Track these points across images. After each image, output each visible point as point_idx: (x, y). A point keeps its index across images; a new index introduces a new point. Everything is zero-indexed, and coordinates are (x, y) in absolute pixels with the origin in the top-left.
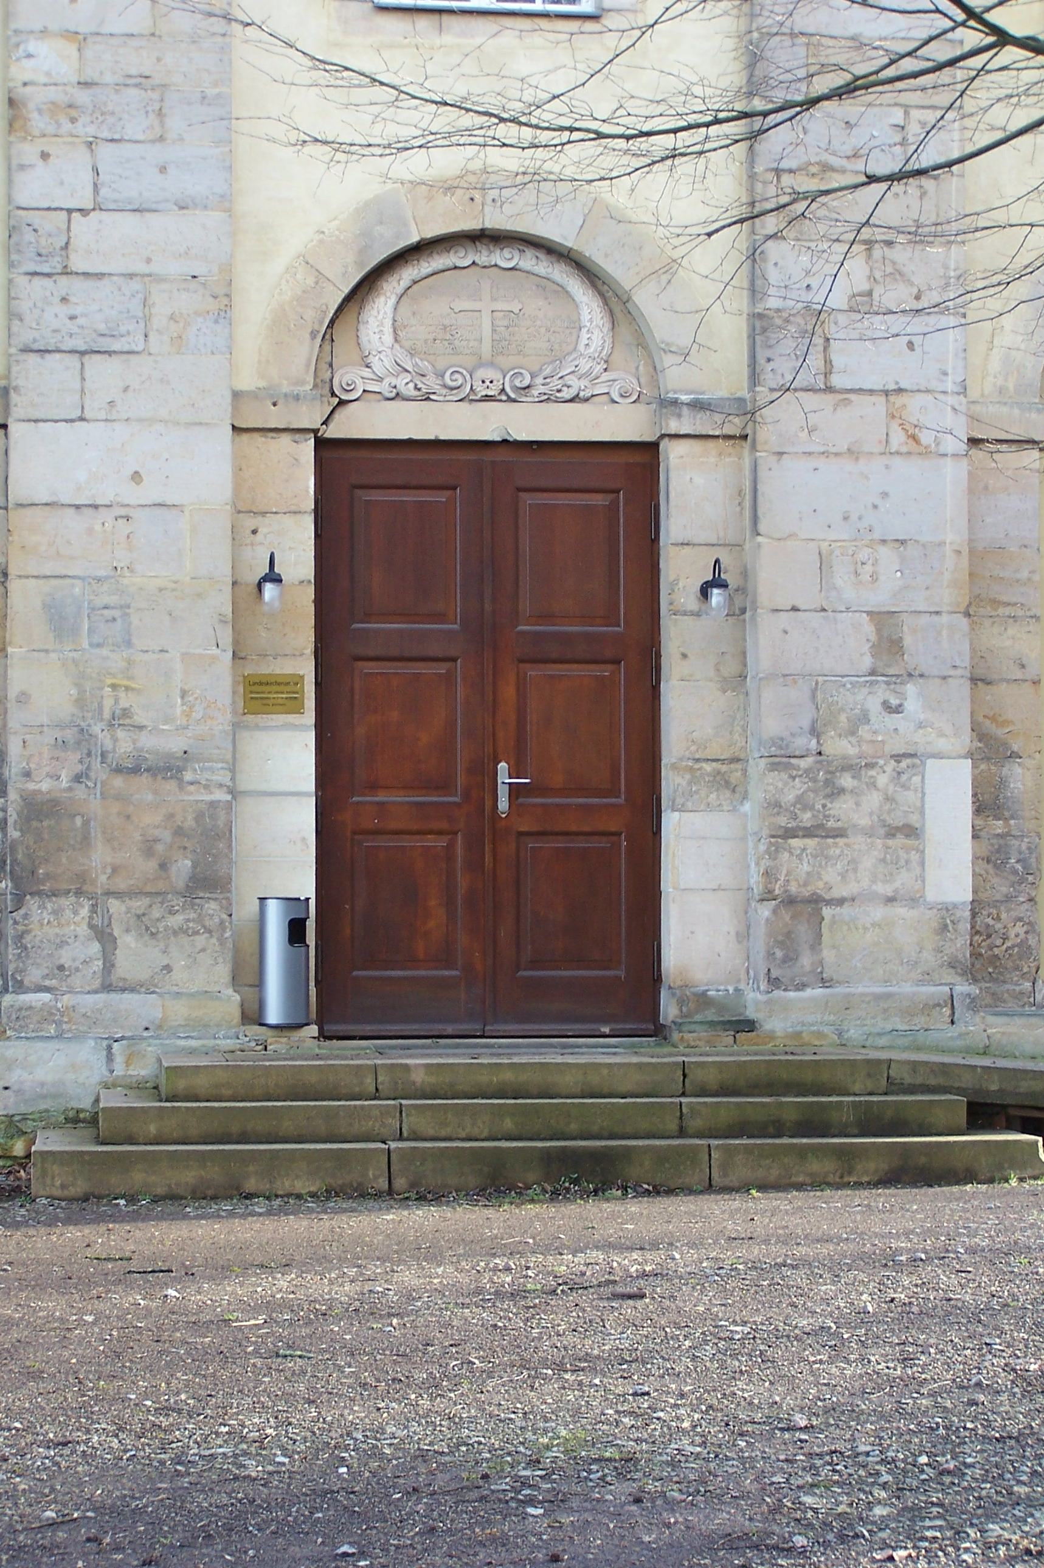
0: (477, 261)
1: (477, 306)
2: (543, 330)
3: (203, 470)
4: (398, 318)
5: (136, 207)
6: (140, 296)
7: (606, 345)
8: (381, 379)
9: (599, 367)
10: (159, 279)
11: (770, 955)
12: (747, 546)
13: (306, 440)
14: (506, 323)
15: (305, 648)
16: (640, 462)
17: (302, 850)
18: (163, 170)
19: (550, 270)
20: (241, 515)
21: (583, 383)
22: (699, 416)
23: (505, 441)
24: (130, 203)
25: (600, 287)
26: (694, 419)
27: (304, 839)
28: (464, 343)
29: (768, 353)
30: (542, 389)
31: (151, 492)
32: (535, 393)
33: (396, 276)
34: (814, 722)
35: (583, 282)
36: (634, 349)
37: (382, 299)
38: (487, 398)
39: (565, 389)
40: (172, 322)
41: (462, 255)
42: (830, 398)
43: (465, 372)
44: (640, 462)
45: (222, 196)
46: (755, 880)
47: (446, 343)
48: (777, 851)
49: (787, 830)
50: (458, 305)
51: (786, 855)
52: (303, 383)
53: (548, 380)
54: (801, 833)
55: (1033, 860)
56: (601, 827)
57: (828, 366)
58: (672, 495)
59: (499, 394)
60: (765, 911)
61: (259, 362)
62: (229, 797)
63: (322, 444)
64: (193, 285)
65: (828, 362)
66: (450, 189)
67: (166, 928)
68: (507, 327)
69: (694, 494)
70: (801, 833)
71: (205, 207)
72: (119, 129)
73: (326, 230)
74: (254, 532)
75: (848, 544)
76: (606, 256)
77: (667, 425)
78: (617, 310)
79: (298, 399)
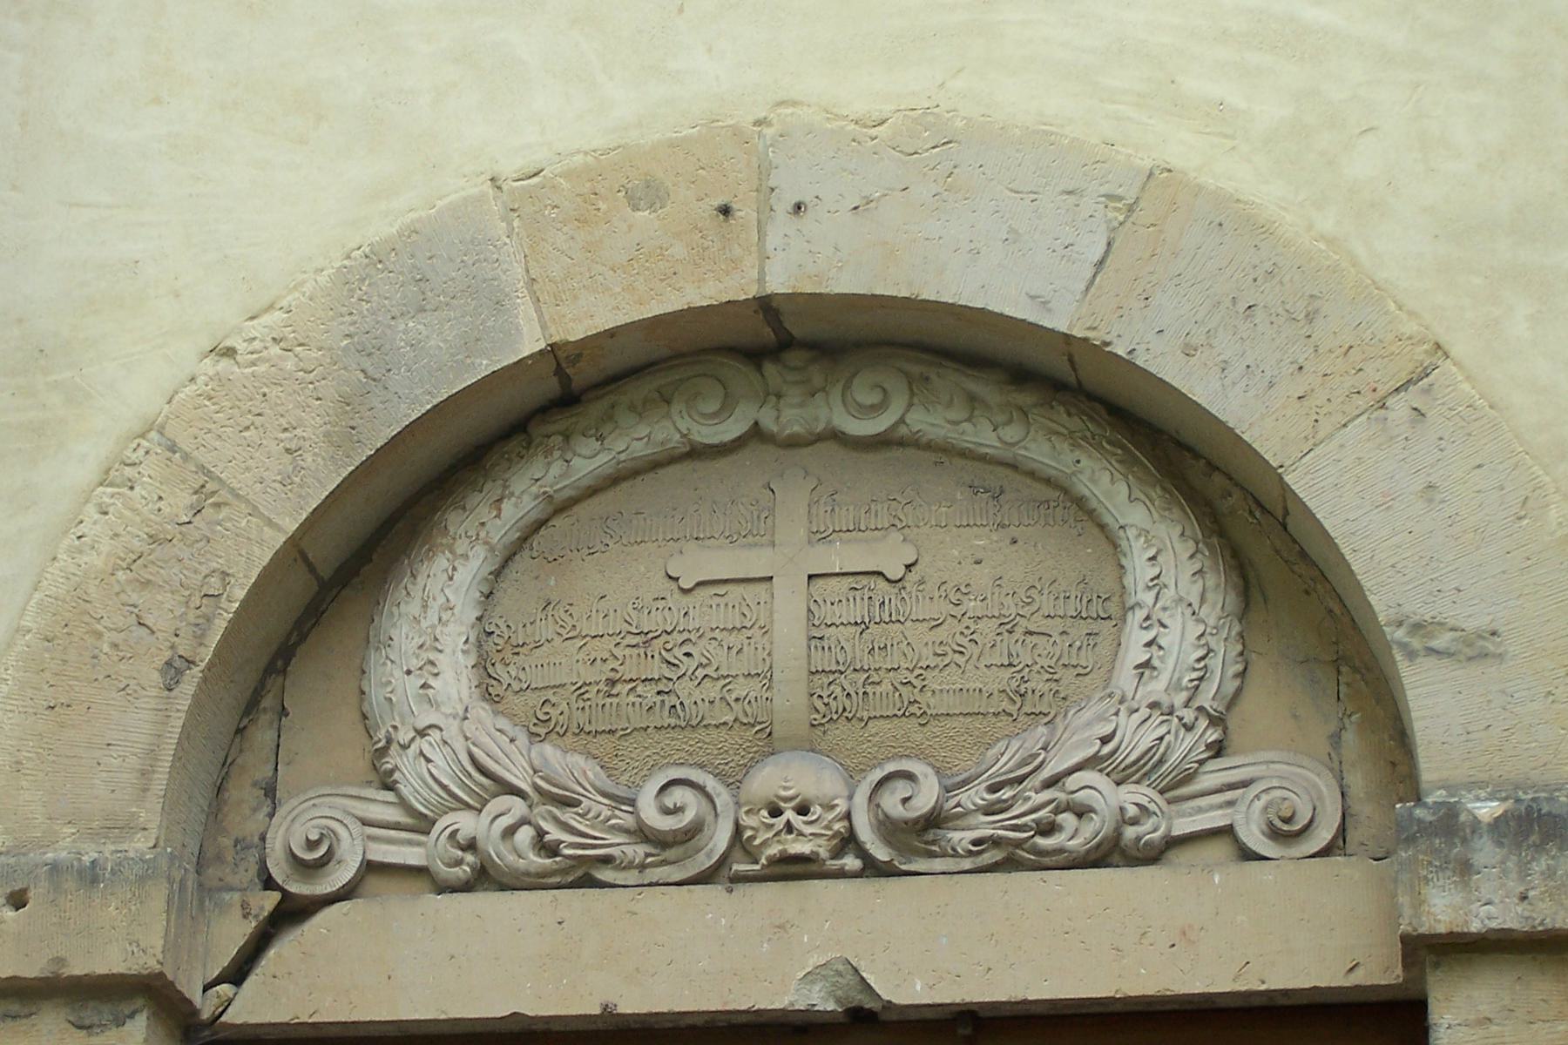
0: (768, 422)
1: (755, 562)
2: (988, 628)
4: (497, 622)
7: (1216, 663)
8: (422, 824)
9: (1189, 739)
13: (119, 1022)
14: (857, 611)
19: (1012, 433)
21: (1132, 796)
22: (1541, 865)
26: (1524, 872)
28: (712, 690)
30: (985, 827)
32: (961, 838)
33: (492, 489)
35: (1128, 462)
37: (442, 562)
38: (793, 868)
39: (1067, 819)
41: (712, 406)
43: (711, 783)
47: (649, 691)
50: (696, 564)
52: (128, 828)
53: (1006, 794)
59: (837, 853)
66: (647, 195)
68: (862, 625)
73: (241, 346)
77: (1419, 903)
79: (95, 881)
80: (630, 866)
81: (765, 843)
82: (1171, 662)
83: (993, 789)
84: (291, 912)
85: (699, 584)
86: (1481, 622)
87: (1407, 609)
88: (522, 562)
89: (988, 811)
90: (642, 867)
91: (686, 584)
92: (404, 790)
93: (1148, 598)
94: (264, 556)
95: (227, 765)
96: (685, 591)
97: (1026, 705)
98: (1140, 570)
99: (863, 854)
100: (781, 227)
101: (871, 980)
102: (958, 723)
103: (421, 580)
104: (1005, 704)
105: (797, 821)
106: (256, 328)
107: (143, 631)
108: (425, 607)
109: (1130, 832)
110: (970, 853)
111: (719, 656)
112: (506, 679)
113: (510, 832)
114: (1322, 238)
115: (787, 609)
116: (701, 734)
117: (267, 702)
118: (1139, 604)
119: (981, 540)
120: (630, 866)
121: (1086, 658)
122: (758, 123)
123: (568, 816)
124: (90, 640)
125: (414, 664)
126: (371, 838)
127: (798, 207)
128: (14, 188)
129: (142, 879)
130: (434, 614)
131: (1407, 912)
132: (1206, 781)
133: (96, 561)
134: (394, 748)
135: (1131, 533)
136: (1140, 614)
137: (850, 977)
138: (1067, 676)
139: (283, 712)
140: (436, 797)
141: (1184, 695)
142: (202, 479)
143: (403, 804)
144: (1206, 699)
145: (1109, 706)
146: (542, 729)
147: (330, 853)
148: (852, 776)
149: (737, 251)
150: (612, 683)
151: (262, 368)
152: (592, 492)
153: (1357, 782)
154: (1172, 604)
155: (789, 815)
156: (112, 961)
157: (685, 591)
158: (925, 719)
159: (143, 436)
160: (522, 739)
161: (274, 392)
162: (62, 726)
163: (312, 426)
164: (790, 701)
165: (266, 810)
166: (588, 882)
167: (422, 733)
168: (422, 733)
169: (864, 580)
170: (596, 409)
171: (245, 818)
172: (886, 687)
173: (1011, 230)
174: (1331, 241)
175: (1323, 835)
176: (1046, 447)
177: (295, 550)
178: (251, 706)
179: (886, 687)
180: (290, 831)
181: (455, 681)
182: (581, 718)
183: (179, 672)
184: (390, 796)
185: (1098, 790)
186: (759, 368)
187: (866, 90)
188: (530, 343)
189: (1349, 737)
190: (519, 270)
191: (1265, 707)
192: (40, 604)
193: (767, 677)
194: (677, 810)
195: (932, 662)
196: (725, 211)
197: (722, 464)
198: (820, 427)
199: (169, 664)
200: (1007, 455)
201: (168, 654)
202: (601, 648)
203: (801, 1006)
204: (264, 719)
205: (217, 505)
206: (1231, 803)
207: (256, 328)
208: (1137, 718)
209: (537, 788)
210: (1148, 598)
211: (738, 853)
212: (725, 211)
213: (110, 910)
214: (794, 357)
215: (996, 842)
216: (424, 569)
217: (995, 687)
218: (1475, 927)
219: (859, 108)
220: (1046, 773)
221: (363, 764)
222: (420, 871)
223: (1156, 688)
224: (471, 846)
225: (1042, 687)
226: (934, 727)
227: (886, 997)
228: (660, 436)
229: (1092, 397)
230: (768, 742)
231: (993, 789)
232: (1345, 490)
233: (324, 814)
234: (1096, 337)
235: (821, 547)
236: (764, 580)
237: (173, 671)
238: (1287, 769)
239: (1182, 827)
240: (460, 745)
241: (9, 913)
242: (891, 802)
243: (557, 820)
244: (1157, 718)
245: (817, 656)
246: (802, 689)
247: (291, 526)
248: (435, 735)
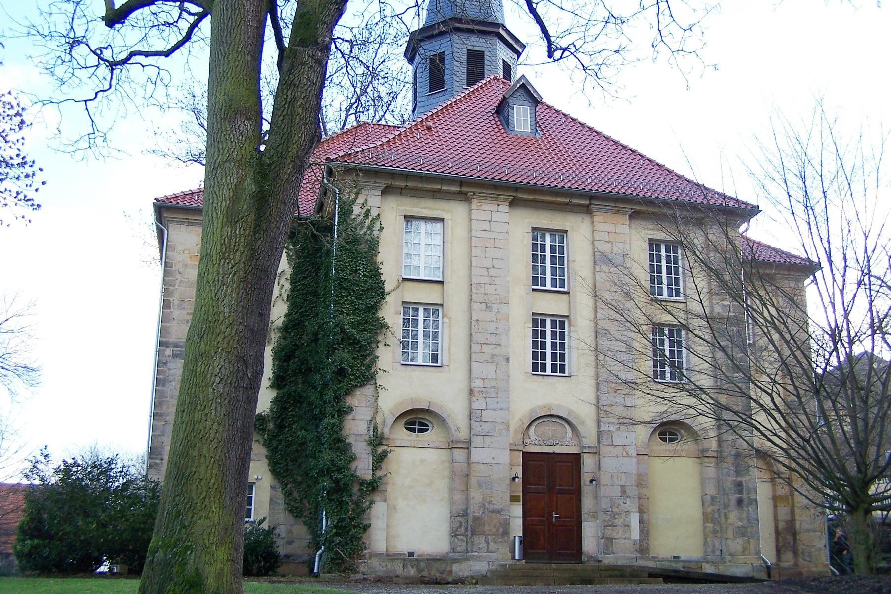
44: (576, 458)
46: (600, 534)
69: (588, 464)
232: (579, 428)
236: (549, 428)
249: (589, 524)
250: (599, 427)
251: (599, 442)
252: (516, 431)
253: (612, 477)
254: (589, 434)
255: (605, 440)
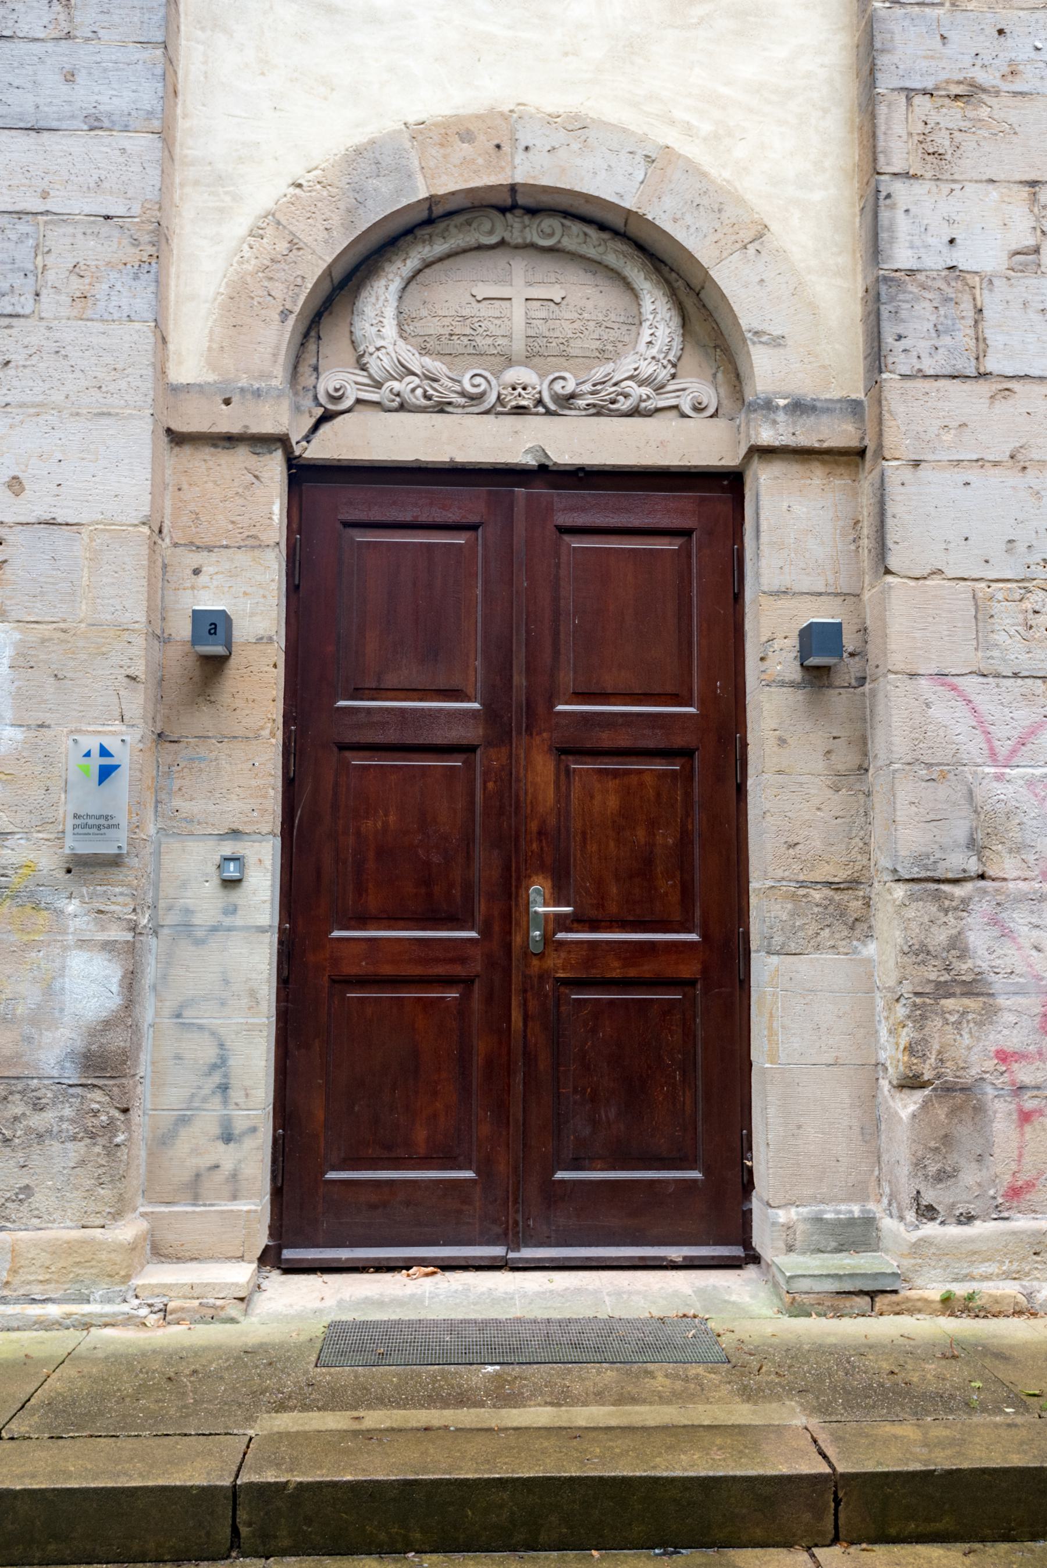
0: (508, 238)
2: (592, 324)
3: (114, 475)
4: (405, 308)
5: (29, 126)
6: (31, 242)
8: (378, 385)
9: (665, 372)
10: (60, 218)
11: (919, 1164)
12: (866, 596)
13: (271, 453)
14: (543, 314)
15: (262, 728)
16: (719, 493)
17: (250, 1008)
18: (70, 77)
20: (178, 550)
21: (645, 391)
22: (801, 421)
23: (543, 468)
24: (21, 120)
25: (667, 275)
27: (252, 993)
28: (489, 341)
29: (900, 330)
31: (35, 505)
32: (581, 403)
34: (973, 831)
36: (711, 351)
37: (383, 282)
38: (520, 410)
39: (621, 398)
40: (74, 278)
42: (984, 388)
44: (719, 493)
45: (149, 113)
46: (891, 1052)
47: (465, 340)
48: (923, 1017)
49: (938, 984)
50: (483, 290)
51: (938, 1022)
52: (270, 376)
53: (599, 387)
54: (958, 991)
55: (193, 863)
56: (670, 972)
57: (982, 346)
58: (764, 526)
60: (906, 1106)
61: (210, 349)
62: (129, 936)
63: (303, 476)
64: (106, 228)
65: (980, 339)
66: (467, 137)
67: (29, 1130)
69: (792, 545)
70: (958, 991)
71: (126, 129)
72: (10, 23)
73: (305, 184)
74: (197, 572)
75: (1014, 585)
76: (675, 220)
77: (757, 434)
78: (689, 303)
79: (259, 396)
80: (459, 406)
81: (510, 400)
82: (659, 342)
83: (594, 385)
84: (327, 417)
85: (485, 299)
86: (779, 333)
87: (753, 326)
88: (413, 286)
89: (592, 393)
90: (464, 407)
91: (479, 299)
92: (372, 371)
93: (651, 317)
94: (319, 272)
95: (298, 357)
96: (479, 301)
97: (603, 355)
98: (647, 306)
99: (545, 407)
100: (520, 157)
101: (549, 454)
102: (580, 360)
103: (375, 288)
104: (597, 354)
105: (523, 392)
106: (311, 176)
107: (270, 298)
108: (377, 299)
109: (643, 405)
110: (585, 409)
111: (492, 328)
112: (409, 331)
113: (413, 390)
114: (725, 180)
115: (518, 311)
116: (484, 357)
117: (313, 333)
118: (648, 319)
119: (589, 291)
120: (459, 406)
121: (626, 339)
122: (511, 111)
123: (435, 385)
124: (249, 300)
125: (374, 322)
126: (358, 389)
127: (527, 148)
128: (204, 105)
129: (279, 396)
130: (380, 305)
131: (753, 436)
132: (669, 388)
133: (249, 268)
134: (367, 355)
135: (645, 292)
136: (648, 323)
137: (541, 453)
138: (620, 345)
139: (319, 338)
140: (384, 375)
141: (663, 355)
142: (291, 237)
143: (370, 376)
144: (671, 357)
145: (637, 357)
146: (424, 351)
147: (343, 394)
148: (542, 376)
149: (504, 164)
150: (451, 335)
151: (314, 194)
152: (441, 260)
153: (722, 391)
154: (658, 321)
155: (520, 390)
156: (268, 428)
157: (479, 301)
158: (568, 357)
159: (266, 217)
160: (417, 355)
161: (319, 204)
162: (239, 334)
163: (336, 220)
164: (518, 346)
165: (315, 376)
166: (442, 411)
167: (378, 349)
168: (378, 349)
169: (546, 303)
170: (442, 225)
171: (307, 379)
172: (554, 344)
173: (609, 166)
174: (728, 182)
175: (711, 411)
176: (614, 256)
177: (329, 271)
178: (306, 335)
179: (554, 344)
180: (328, 383)
181: (390, 329)
182: (438, 348)
183: (286, 315)
184: (365, 373)
185: (631, 386)
186: (504, 215)
187: (553, 102)
188: (423, 194)
189: (720, 375)
190: (416, 163)
191: (691, 361)
192: (227, 283)
193: (509, 337)
194: (479, 385)
195: (572, 335)
196: (498, 147)
197: (491, 253)
198: (528, 241)
199: (282, 312)
200: (598, 258)
201: (281, 308)
202: (446, 321)
203: (524, 462)
204: (312, 340)
205: (299, 249)
206: (678, 397)
207: (311, 176)
208: (647, 362)
209: (424, 374)
210: (651, 317)
211: (498, 404)
212: (498, 147)
213: (266, 408)
214: (518, 212)
215: (594, 406)
216: (376, 284)
217: (594, 347)
218: (777, 444)
219: (550, 109)
220: (614, 381)
221: (353, 360)
222: (377, 404)
223: (654, 351)
224: (398, 395)
225: (611, 349)
226: (571, 361)
227: (555, 460)
228: (468, 239)
229: (629, 239)
230: (509, 362)
231: (594, 385)
232: (734, 280)
233: (337, 377)
234: (640, 212)
235: (530, 288)
236: (512, 300)
237: (285, 314)
238: (698, 387)
239: (661, 404)
240: (394, 355)
241: (224, 407)
242: (558, 387)
243: (431, 387)
244: (654, 363)
245: (529, 330)
246: (523, 342)
247: (329, 260)
248: (383, 351)
249: (807, 968)
250: (874, 244)
251: (876, 358)
252: (238, 300)
253: (981, 614)
254: (799, 321)
255: (919, 334)
